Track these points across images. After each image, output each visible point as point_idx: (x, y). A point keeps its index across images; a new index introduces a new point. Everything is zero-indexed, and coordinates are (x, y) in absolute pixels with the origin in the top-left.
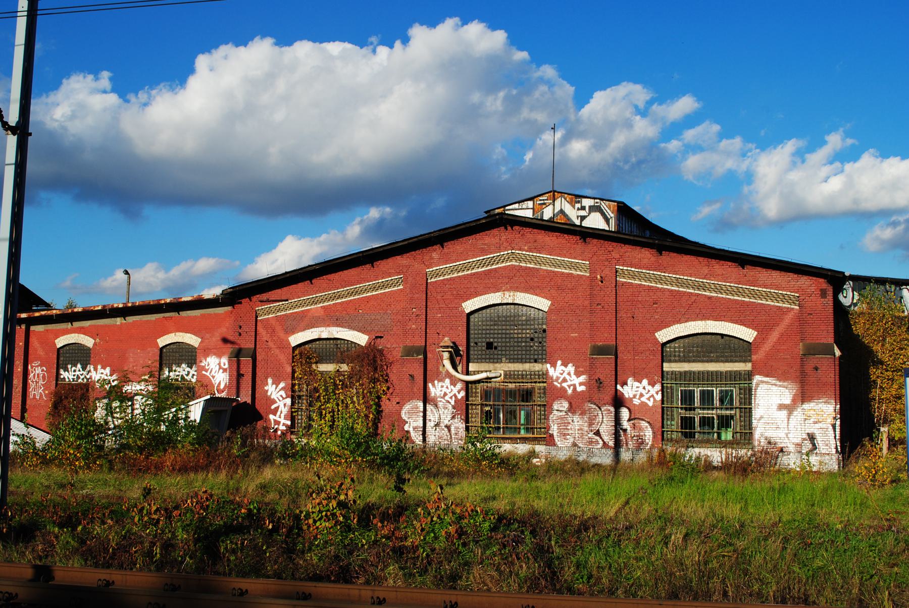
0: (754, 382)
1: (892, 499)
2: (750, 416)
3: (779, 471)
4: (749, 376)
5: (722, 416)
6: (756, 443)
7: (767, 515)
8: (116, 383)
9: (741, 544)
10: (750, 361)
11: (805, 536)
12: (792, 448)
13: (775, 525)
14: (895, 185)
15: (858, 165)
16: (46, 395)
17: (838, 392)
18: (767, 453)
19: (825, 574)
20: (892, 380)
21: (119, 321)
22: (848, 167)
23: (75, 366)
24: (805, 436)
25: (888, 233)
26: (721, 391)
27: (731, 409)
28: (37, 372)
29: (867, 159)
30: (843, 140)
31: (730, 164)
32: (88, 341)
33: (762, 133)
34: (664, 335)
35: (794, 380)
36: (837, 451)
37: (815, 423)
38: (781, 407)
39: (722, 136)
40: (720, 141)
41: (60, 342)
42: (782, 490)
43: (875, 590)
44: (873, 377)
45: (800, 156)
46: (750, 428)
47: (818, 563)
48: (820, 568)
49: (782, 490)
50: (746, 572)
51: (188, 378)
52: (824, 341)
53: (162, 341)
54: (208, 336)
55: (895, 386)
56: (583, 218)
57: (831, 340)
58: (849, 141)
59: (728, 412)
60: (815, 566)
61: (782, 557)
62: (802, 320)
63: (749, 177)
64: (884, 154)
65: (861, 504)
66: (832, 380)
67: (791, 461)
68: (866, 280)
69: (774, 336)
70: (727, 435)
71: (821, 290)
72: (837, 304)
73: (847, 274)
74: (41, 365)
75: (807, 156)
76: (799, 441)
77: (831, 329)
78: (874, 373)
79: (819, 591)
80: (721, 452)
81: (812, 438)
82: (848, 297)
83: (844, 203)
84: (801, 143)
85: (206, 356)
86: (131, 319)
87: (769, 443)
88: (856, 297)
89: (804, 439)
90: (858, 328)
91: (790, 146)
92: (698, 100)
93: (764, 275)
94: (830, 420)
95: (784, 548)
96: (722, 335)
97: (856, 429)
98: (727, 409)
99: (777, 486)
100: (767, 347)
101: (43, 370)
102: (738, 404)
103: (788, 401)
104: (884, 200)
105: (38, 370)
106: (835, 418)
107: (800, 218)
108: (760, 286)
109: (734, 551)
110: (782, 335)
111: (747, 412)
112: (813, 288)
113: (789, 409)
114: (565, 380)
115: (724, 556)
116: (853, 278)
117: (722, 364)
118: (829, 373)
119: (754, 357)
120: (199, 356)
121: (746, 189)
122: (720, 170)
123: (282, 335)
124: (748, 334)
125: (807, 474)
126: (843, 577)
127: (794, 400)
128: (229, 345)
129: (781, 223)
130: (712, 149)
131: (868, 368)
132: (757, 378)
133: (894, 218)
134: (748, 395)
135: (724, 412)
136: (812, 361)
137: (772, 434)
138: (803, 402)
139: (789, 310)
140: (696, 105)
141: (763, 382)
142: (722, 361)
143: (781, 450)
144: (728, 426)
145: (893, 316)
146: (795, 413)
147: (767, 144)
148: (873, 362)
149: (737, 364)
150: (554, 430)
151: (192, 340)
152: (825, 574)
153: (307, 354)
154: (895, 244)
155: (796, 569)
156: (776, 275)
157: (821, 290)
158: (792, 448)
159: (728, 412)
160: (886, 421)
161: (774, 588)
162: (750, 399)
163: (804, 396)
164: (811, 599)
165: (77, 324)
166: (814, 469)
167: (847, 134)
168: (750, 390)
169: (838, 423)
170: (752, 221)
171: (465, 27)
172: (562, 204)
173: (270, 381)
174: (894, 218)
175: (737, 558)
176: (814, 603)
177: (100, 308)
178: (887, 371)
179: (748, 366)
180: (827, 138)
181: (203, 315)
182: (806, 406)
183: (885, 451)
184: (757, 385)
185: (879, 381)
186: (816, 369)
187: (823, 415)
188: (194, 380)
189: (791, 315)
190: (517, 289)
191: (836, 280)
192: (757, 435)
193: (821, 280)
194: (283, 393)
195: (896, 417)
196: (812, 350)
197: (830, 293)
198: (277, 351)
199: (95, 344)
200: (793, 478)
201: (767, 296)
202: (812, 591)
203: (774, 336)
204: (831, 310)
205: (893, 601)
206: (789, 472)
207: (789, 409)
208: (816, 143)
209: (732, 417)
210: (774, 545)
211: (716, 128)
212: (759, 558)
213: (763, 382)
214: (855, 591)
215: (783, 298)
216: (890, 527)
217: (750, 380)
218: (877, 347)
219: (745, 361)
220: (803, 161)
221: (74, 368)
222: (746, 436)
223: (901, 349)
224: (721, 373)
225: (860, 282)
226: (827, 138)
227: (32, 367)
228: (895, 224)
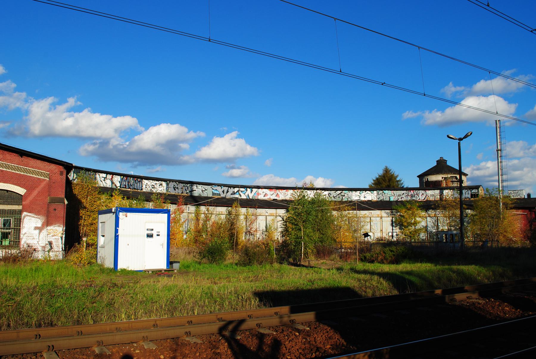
0: (23, 215)
1: (90, 272)
2: (19, 233)
3: (32, 260)
4: (20, 212)
5: (4, 233)
6: (22, 246)
7: (30, 282)
9: (18, 299)
10: (21, 205)
11: (52, 292)
12: (40, 249)
13: (34, 287)
14: (96, 126)
15: (81, 114)
17: (65, 221)
18: (27, 251)
19: (61, 310)
20: (90, 216)
22: (76, 115)
24: (47, 243)
25: (91, 148)
26: (5, 220)
27: (10, 229)
29: (86, 112)
30: (76, 102)
31: (18, 104)
33: (37, 91)
35: (43, 215)
36: (62, 250)
37: (53, 236)
38: (36, 228)
39: (16, 90)
40: (15, 92)
42: (37, 270)
43: (85, 315)
44: (81, 215)
45: (53, 107)
46: (19, 239)
47: (58, 305)
48: (59, 307)
49: (37, 270)
50: (20, 313)
52: (60, 196)
55: (91, 219)
57: (63, 196)
58: (79, 103)
59: (7, 231)
60: (56, 306)
61: (40, 304)
62: (50, 186)
63: (27, 113)
64: (94, 111)
65: (76, 275)
66: (62, 216)
67: (39, 255)
68: (82, 169)
70: (6, 243)
71: (61, 172)
72: (67, 179)
73: (74, 165)
75: (57, 106)
76: (44, 245)
77: (64, 191)
78: (82, 212)
79: (58, 319)
80: (2, 251)
81: (50, 243)
82: (72, 176)
83: (73, 131)
84: (56, 100)
87: (29, 246)
88: (75, 176)
89: (47, 244)
90: (76, 191)
91: (50, 100)
92: (6, 70)
93: (32, 161)
94: (60, 235)
95: (41, 299)
96: (7, 191)
97: (72, 239)
98: (7, 229)
99: (34, 268)
100: (31, 198)
102: (13, 227)
103: (39, 225)
104: (90, 132)
106: (62, 234)
107: (50, 135)
108: (30, 167)
109: (15, 303)
110: (39, 192)
111: (18, 231)
112: (57, 170)
113: (40, 229)
115: (9, 306)
116: (76, 168)
117: (6, 206)
118: (61, 211)
119: (24, 203)
121: (24, 118)
122: (13, 107)
124: (21, 191)
125: (47, 261)
126: (70, 311)
127: (43, 225)
129: (42, 137)
130: (10, 95)
131: (79, 210)
132: (25, 213)
133: (94, 141)
134: (19, 222)
135: (5, 231)
136: (53, 206)
137: (31, 242)
138: (47, 226)
139: (44, 180)
140: (4, 71)
141: (27, 215)
142: (6, 204)
143: (35, 250)
144: (7, 238)
145: (93, 187)
146: (43, 231)
147: (39, 97)
148: (82, 207)
149: (14, 206)
152: (61, 310)
154: (93, 153)
155: (47, 309)
156: (39, 163)
157: (61, 172)
158: (40, 249)
159: (7, 231)
160: (86, 235)
161: (35, 319)
162: (20, 224)
163: (48, 223)
164: (54, 323)
166: (51, 259)
167: (78, 100)
168: (20, 219)
169: (64, 236)
170: (26, 134)
171: (148, 131)
174: (94, 141)
175: (16, 306)
176: (55, 324)
178: (87, 211)
179: (20, 207)
180: (68, 100)
182: (49, 228)
183: (85, 250)
184: (24, 217)
185: (84, 216)
186: (55, 210)
187: (57, 233)
189: (45, 183)
191: (68, 167)
192: (22, 242)
193: (61, 167)
195: (91, 234)
196: (54, 201)
197: (65, 173)
200: (42, 264)
201: (33, 172)
202: (54, 319)
203: (35, 193)
204: (65, 182)
205: (93, 320)
206: (38, 260)
207: (40, 229)
208: (63, 101)
209: (9, 233)
210: (36, 298)
211: (14, 85)
212: (28, 305)
213: (27, 215)
214: (75, 317)
215: (41, 174)
216: (91, 285)
217: (21, 214)
218: (83, 201)
219: (19, 205)
220: (55, 109)
222: (16, 243)
223: (95, 202)
224: (5, 210)
225: (78, 169)
226: (68, 100)
228: (95, 144)
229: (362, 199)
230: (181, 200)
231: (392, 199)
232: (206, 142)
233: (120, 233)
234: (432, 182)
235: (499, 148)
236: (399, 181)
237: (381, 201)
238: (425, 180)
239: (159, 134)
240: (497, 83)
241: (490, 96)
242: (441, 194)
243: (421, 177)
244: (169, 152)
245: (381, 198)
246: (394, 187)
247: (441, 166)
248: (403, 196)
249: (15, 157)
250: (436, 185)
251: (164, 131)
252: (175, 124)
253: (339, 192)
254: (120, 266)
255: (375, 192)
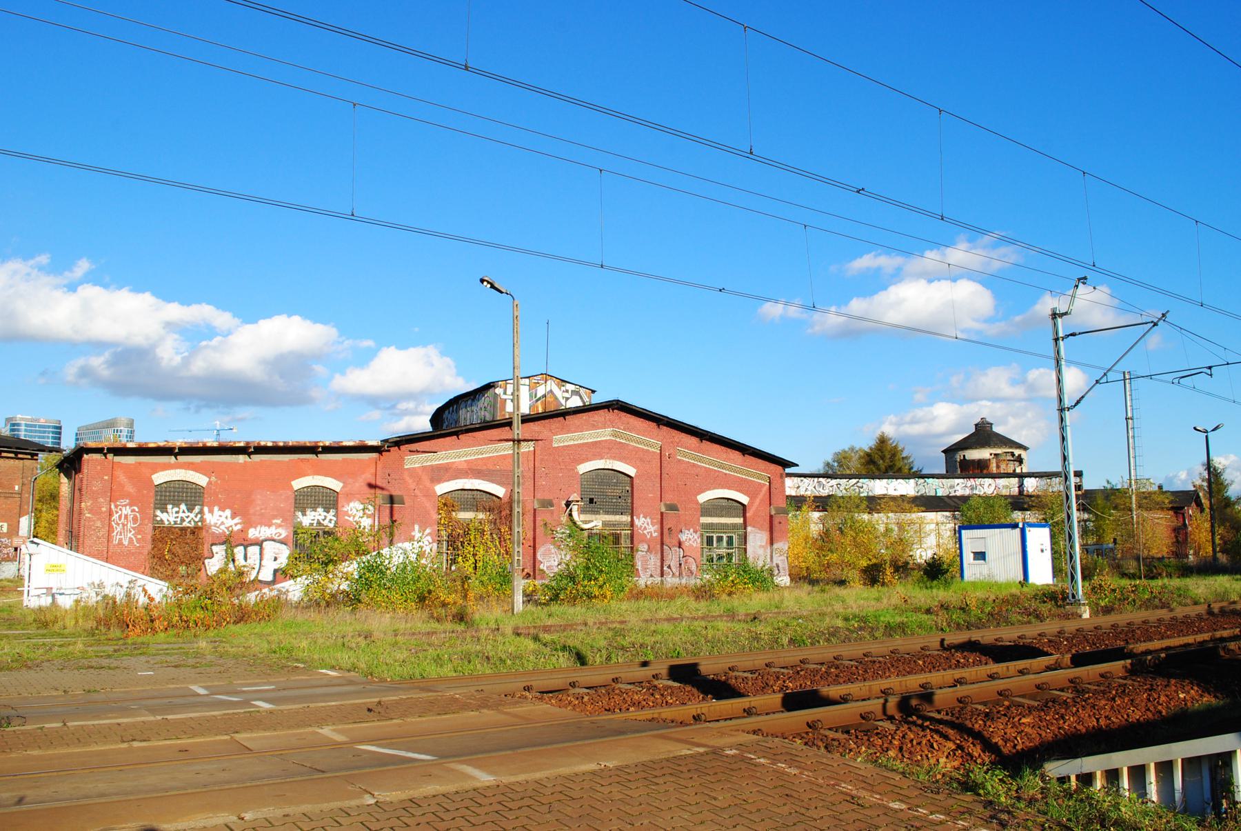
4: (745, 525)
8: (239, 527)
16: (138, 540)
21: (242, 458)
23: (178, 506)
28: (124, 512)
32: (202, 480)
34: (703, 498)
38: (761, 546)
41: (159, 478)
51: (325, 523)
53: (298, 484)
54: (350, 481)
56: (567, 399)
69: (757, 501)
74: (131, 505)
85: (348, 502)
86: (257, 458)
101: (133, 511)
105: (127, 511)
114: (183, 520)
120: (341, 501)
123: (428, 483)
124: (744, 499)
128: (378, 491)
150: (639, 566)
151: (334, 484)
153: (449, 503)
165: (182, 459)
172: (552, 385)
173: (417, 527)
177: (242, 444)
181: (344, 460)
188: (332, 525)
190: (614, 458)
194: (429, 538)
198: (424, 499)
199: (210, 483)
203: (757, 501)
221: (176, 509)
227: (116, 506)
229: (892, 493)
230: (810, 501)
231: (939, 494)
232: (363, 359)
233: (1028, 549)
234: (973, 461)
235: (1129, 415)
236: (906, 458)
237: (922, 496)
238: (959, 456)
239: (257, 342)
240: (958, 255)
241: (943, 282)
242: (1021, 486)
243: (950, 452)
244: (289, 379)
245: (922, 492)
246: (900, 469)
247: (983, 435)
248: (957, 488)
249: (736, 455)
250: (978, 469)
251: (289, 332)
252: (144, 292)
253: (854, 481)
254: (1031, 580)
255: (912, 481)
